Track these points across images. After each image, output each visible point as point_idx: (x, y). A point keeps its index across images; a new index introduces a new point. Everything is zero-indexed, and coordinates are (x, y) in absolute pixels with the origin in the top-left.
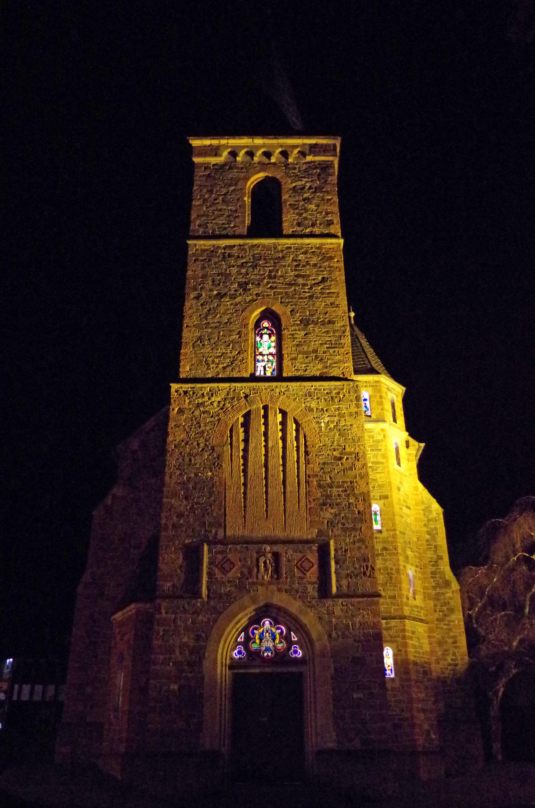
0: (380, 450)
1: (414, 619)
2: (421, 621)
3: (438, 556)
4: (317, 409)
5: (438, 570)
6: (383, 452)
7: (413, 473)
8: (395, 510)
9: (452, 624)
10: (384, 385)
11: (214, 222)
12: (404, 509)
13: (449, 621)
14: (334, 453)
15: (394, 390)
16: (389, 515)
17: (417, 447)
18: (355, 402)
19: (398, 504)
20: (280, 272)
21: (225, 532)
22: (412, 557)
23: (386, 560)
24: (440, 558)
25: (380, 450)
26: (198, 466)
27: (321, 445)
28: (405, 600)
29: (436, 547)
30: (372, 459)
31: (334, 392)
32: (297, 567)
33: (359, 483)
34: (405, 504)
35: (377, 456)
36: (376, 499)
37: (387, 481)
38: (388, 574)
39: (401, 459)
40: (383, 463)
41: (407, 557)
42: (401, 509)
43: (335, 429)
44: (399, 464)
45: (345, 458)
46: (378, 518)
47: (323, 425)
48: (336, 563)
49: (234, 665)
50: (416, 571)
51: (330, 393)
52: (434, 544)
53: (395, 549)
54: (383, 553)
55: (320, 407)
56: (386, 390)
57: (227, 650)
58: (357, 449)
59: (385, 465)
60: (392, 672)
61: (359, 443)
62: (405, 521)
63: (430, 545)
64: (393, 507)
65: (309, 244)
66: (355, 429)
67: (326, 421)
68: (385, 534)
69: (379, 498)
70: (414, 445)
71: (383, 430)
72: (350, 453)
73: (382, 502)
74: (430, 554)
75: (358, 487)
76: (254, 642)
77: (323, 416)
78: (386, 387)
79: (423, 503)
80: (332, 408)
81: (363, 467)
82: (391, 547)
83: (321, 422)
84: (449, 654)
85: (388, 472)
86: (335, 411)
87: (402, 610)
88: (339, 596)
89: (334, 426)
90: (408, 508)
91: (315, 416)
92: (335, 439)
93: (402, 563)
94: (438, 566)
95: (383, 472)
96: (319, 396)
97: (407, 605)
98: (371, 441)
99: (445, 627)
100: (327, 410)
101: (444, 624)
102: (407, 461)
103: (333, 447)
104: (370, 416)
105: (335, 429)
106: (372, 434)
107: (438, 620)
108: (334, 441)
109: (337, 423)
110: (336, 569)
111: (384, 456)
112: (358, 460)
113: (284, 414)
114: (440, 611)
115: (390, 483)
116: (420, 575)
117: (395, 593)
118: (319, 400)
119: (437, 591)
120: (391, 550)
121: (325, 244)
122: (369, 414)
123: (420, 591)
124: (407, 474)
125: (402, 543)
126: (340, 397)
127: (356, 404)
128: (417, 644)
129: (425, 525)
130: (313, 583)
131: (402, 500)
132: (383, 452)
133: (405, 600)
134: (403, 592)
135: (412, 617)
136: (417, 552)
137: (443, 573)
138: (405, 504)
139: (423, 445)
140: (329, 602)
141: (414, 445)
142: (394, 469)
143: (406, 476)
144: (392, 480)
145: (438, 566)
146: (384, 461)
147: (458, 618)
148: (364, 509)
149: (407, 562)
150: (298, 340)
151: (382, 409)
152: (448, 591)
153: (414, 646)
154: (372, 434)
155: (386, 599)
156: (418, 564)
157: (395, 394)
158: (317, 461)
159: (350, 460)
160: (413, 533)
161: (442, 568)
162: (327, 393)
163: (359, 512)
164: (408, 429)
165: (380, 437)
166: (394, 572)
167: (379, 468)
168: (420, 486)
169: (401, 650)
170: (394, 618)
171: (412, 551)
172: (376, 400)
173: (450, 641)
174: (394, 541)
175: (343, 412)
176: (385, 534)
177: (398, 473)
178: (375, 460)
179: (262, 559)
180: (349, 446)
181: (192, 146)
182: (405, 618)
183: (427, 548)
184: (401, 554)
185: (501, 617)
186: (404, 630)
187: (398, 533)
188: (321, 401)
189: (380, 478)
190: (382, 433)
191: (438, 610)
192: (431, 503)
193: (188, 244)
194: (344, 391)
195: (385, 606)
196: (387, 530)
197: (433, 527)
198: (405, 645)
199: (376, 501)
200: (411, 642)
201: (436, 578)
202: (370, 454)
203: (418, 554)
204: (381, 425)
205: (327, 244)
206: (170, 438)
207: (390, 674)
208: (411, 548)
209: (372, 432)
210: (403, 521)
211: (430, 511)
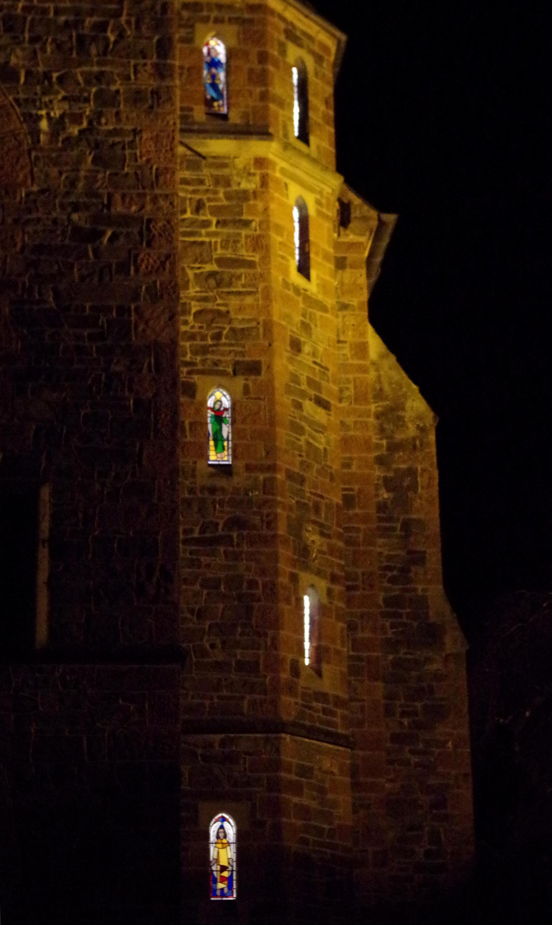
0: (246, 224)
1: (311, 732)
2: (334, 738)
3: (410, 552)
4: (29, 74)
5: (407, 595)
6: (254, 229)
7: (355, 302)
8: (278, 408)
10: (276, 20)
12: (309, 406)
14: (75, 217)
15: (310, 38)
16: (254, 422)
17: (374, 223)
18: (155, 59)
19: (289, 390)
22: (320, 552)
23: (237, 557)
24: (418, 559)
25: (246, 224)
27: (35, 188)
28: (285, 676)
29: (406, 525)
30: (219, 251)
31: (89, 21)
33: (147, 315)
34: (312, 393)
35: (236, 242)
36: (223, 374)
37: (261, 319)
38: (240, 597)
39: (312, 256)
40: (251, 265)
41: (304, 551)
42: (299, 406)
43: (84, 143)
44: (304, 269)
45: (109, 233)
46: (226, 430)
47: (44, 125)
50: (329, 592)
51: (77, 24)
52: (401, 518)
53: (269, 524)
54: (231, 538)
55: (41, 69)
56: (282, 38)
58: (149, 207)
59: (259, 270)
60: (230, 887)
61: (157, 191)
62: (308, 444)
63: (390, 519)
64: (272, 402)
66: (146, 145)
67: (56, 113)
68: (239, 480)
69: (230, 370)
70: (365, 219)
71: (260, 162)
72: (125, 220)
73: (240, 381)
74: (382, 547)
75: (141, 328)
77: (46, 99)
78: (282, 26)
79: (379, 395)
80: (79, 73)
81: (163, 264)
82: (257, 520)
83: (40, 118)
85: (267, 296)
86: (88, 82)
87: (275, 703)
89: (81, 132)
90: (321, 403)
91: (22, 96)
92: (82, 173)
93: (284, 567)
94: (409, 581)
95: (250, 293)
96: (40, 30)
97: (291, 689)
98: (221, 195)
99: (415, 759)
100: (60, 80)
101: (412, 752)
102: (331, 266)
103: (73, 199)
104: (225, 117)
105: (84, 143)
106: (226, 171)
107: (395, 738)
108: (77, 179)
109: (90, 123)
110: (51, 576)
111: (259, 243)
112: (149, 245)
114: (404, 714)
115: (268, 326)
116: (341, 605)
118: (37, 46)
120: (254, 527)
122: (224, 110)
123: (338, 652)
124: (330, 302)
125: (291, 509)
126: (107, 39)
127: (156, 66)
128: (314, 804)
129: (381, 461)
131: (303, 379)
132: (254, 229)
133: (285, 676)
134: (282, 654)
135: (303, 726)
136: (340, 536)
137: (422, 602)
138: (312, 393)
139: (391, 218)
141: (365, 219)
142: (286, 284)
143: (324, 309)
144: (275, 318)
145: (409, 581)
146: (256, 258)
147: (453, 734)
148: (156, 395)
149: (306, 567)
151: (264, 96)
153: (304, 812)
154: (226, 171)
156: (336, 571)
157: (311, 52)
158: (18, 240)
159: (122, 240)
160: (332, 479)
161: (420, 587)
162: (66, 23)
163: (138, 403)
164: (342, 166)
165: (249, 185)
166: (259, 592)
167: (239, 277)
168: (374, 343)
170: (250, 728)
171: (322, 534)
172: (247, 67)
174: (266, 502)
175: (113, 88)
176: (239, 480)
177: (300, 299)
178: (229, 254)
180: (123, 197)
182: (281, 727)
183: (378, 528)
184: (286, 541)
185: (196, 657)
186: (276, 765)
187: (280, 476)
188: (43, 50)
189: (240, 309)
190: (258, 172)
192: (405, 396)
194: (123, 19)
195: (225, 693)
196: (248, 468)
197: (403, 466)
199: (223, 380)
200: (296, 800)
201: (400, 616)
202: (216, 234)
203: (340, 544)
204: (257, 148)
207: (225, 890)
208: (321, 525)
209: (225, 166)
210: (302, 443)
211: (400, 419)
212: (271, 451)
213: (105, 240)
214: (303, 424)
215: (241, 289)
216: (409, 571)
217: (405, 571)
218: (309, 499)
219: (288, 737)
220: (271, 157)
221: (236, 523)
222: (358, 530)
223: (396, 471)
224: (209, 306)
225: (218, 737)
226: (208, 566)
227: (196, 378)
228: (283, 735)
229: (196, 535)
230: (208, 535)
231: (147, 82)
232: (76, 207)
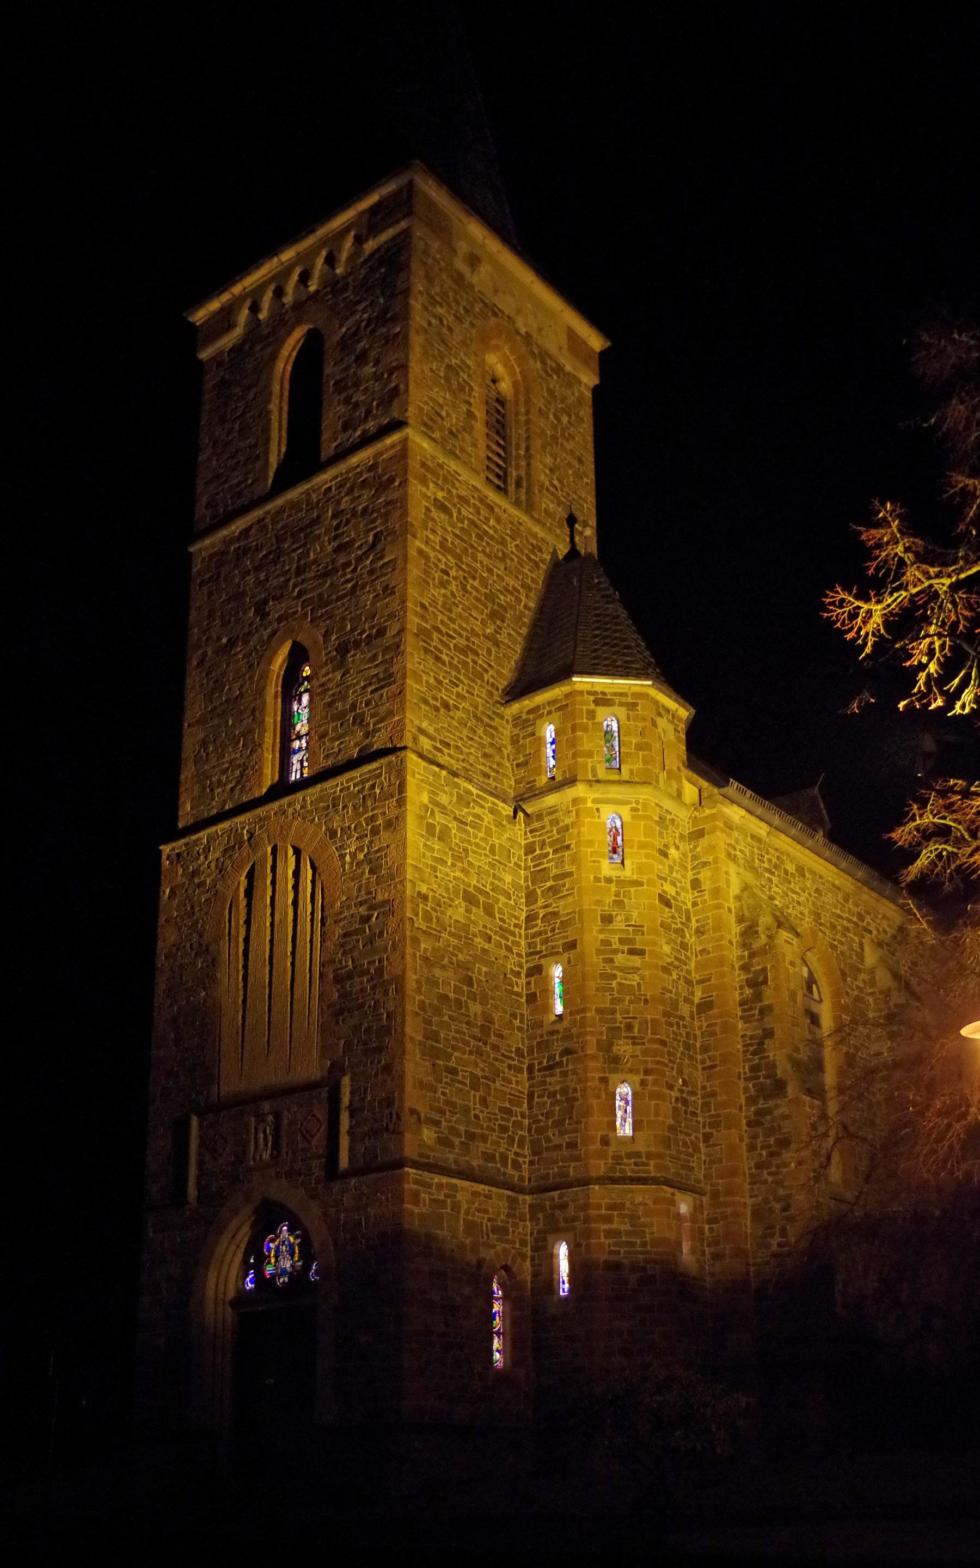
0: (568, 847)
3: (764, 1030)
9: (785, 1170)
11: (226, 486)
13: (778, 1167)
14: (361, 910)
20: (312, 554)
21: (219, 1089)
25: (568, 847)
26: (189, 985)
27: (344, 899)
29: (762, 1012)
32: (301, 1132)
36: (558, 953)
40: (571, 874)
48: (352, 1116)
49: (242, 1299)
57: (227, 1277)
65: (358, 466)
67: (353, 849)
73: (566, 955)
76: (269, 1263)
84: (774, 1235)
88: (353, 1172)
98: (555, 832)
99: (770, 1179)
113: (297, 852)
114: (762, 1148)
117: (576, 1137)
119: (760, 1106)
121: (381, 454)
130: (320, 1157)
140: (336, 1186)
150: (330, 693)
152: (779, 1102)
155: (562, 1150)
161: (771, 1054)
167: (564, 885)
169: (580, 1245)
173: (778, 1206)
179: (261, 1126)
181: (197, 327)
188: (348, 813)
191: (759, 1145)
193: (191, 553)
194: (383, 778)
195: (561, 1164)
198: (588, 1233)
205: (387, 450)
206: (160, 944)
209: (556, 811)
212: (584, 998)
213: (374, 919)
214: (614, 972)
215: (566, 893)
216: (763, 1044)
217: (761, 1044)
218: (621, 1023)
219: (597, 1187)
220: (581, 795)
221: (567, 1052)
222: (715, 1024)
223: (755, 972)
224: (550, 910)
225: (555, 1194)
226: (550, 1084)
227: (542, 961)
228: (591, 1186)
229: (545, 1064)
230: (551, 1063)
231: (392, 813)
232: (361, 904)
